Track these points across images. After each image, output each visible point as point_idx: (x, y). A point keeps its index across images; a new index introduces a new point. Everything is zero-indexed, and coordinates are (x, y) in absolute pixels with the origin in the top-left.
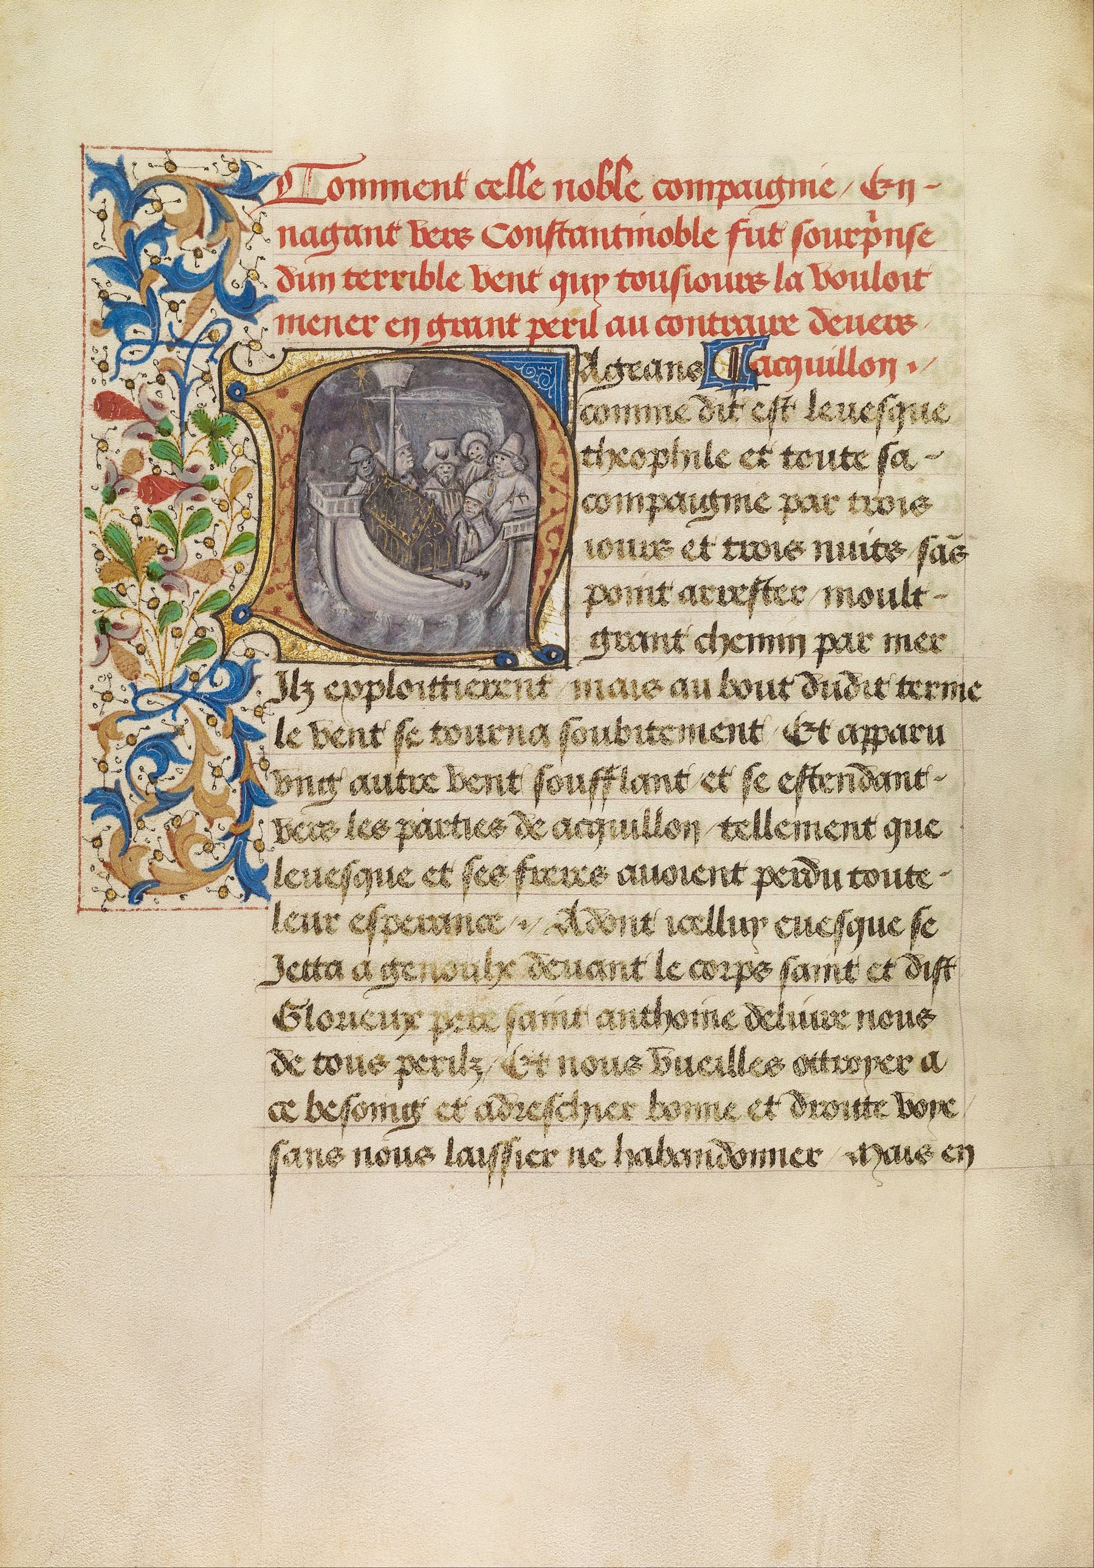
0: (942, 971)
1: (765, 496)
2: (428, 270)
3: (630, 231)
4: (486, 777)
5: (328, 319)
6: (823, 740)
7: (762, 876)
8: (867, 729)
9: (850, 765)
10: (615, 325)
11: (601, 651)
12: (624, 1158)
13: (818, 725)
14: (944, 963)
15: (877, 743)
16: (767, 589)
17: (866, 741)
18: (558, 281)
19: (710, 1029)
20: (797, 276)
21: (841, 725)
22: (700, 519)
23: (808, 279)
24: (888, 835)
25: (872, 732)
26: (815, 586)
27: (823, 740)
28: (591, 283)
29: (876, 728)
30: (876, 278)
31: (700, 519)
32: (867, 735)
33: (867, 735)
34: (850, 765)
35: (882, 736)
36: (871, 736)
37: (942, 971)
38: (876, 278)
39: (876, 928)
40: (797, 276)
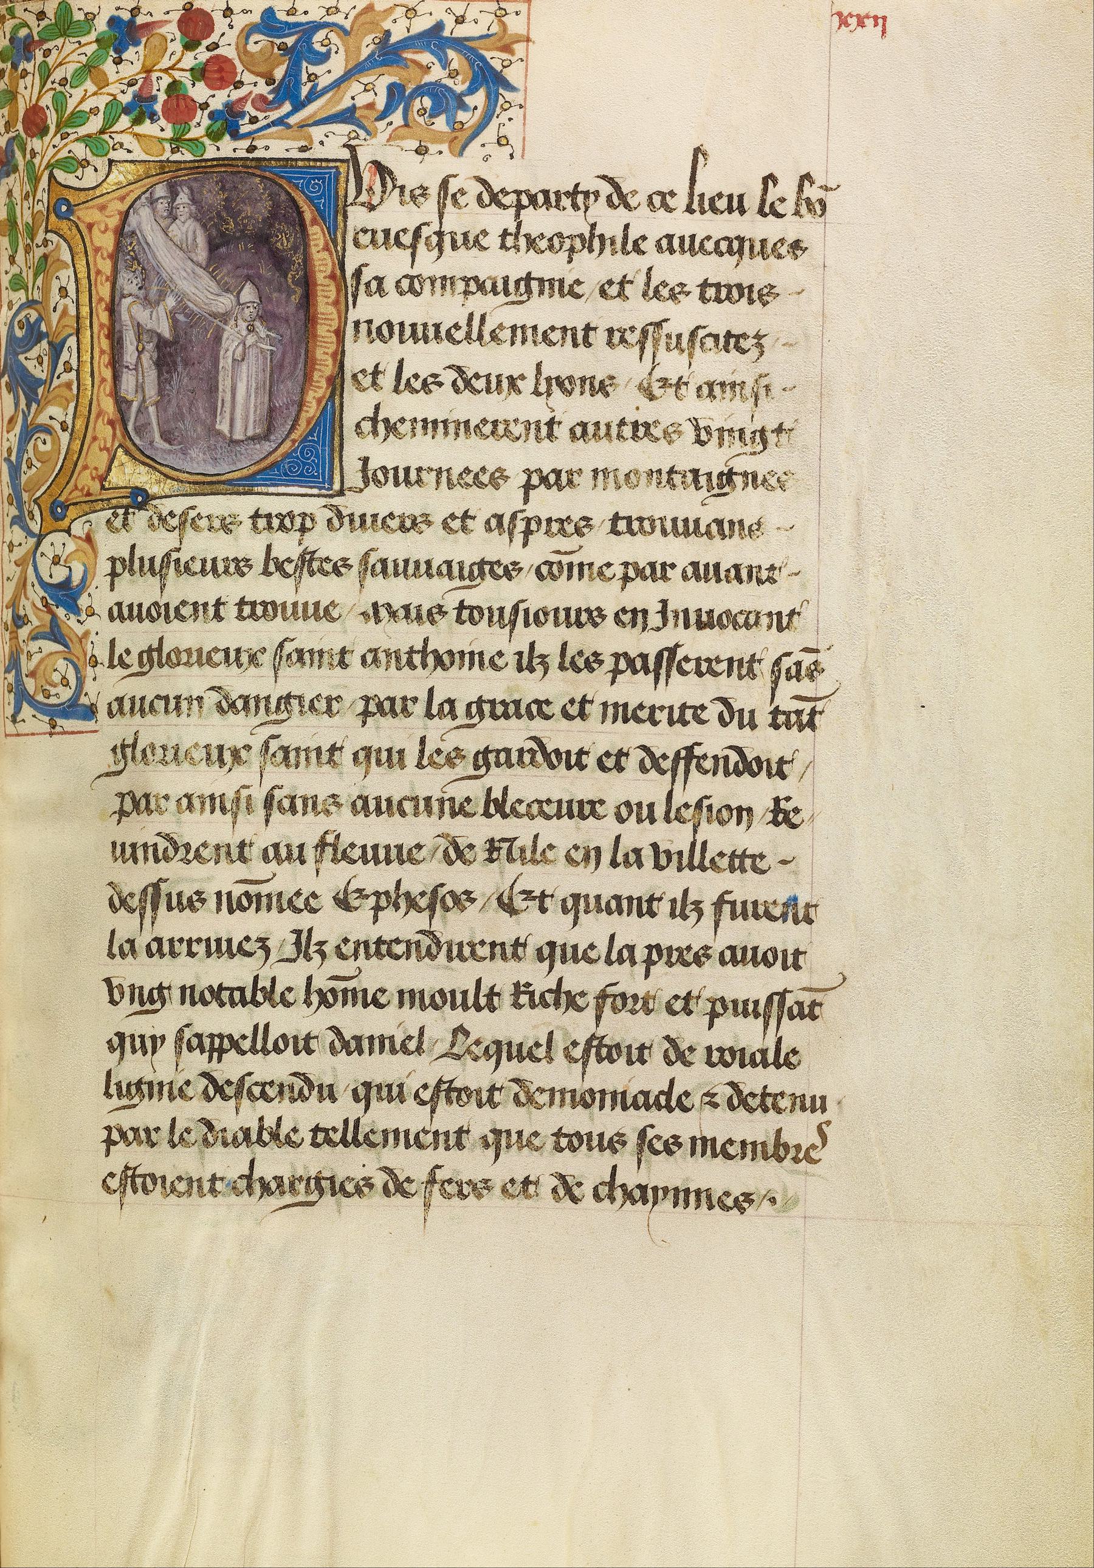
0: (593, 1050)
1: (485, 233)
2: (493, 796)
3: (541, 281)
4: (515, 192)
5: (743, 1143)
6: (543, 910)
7: (529, 477)
8: (212, 1036)
9: (331, 978)
10: (360, 803)
11: (476, 719)
12: (315, 999)
13: (537, 893)
14: (595, 1043)
15: (222, 1051)
16: (599, 1048)
17: (212, 1050)
18: (362, 1092)
19: (567, 1108)
20: (637, 851)
21: (542, 942)
22: (513, 303)
23: (647, 854)
24: (565, 911)
25: (217, 1041)
26: (354, 623)
27: (543, 910)
28: (149, 1044)
29: (221, 1036)
30: (534, 851)
31: (513, 303)
32: (212, 1043)
33: (212, 1043)
34: (331, 978)
35: (226, 1044)
36: (216, 1046)
37: (593, 1050)
38: (534, 851)
39: (569, 955)
40: (637, 851)
